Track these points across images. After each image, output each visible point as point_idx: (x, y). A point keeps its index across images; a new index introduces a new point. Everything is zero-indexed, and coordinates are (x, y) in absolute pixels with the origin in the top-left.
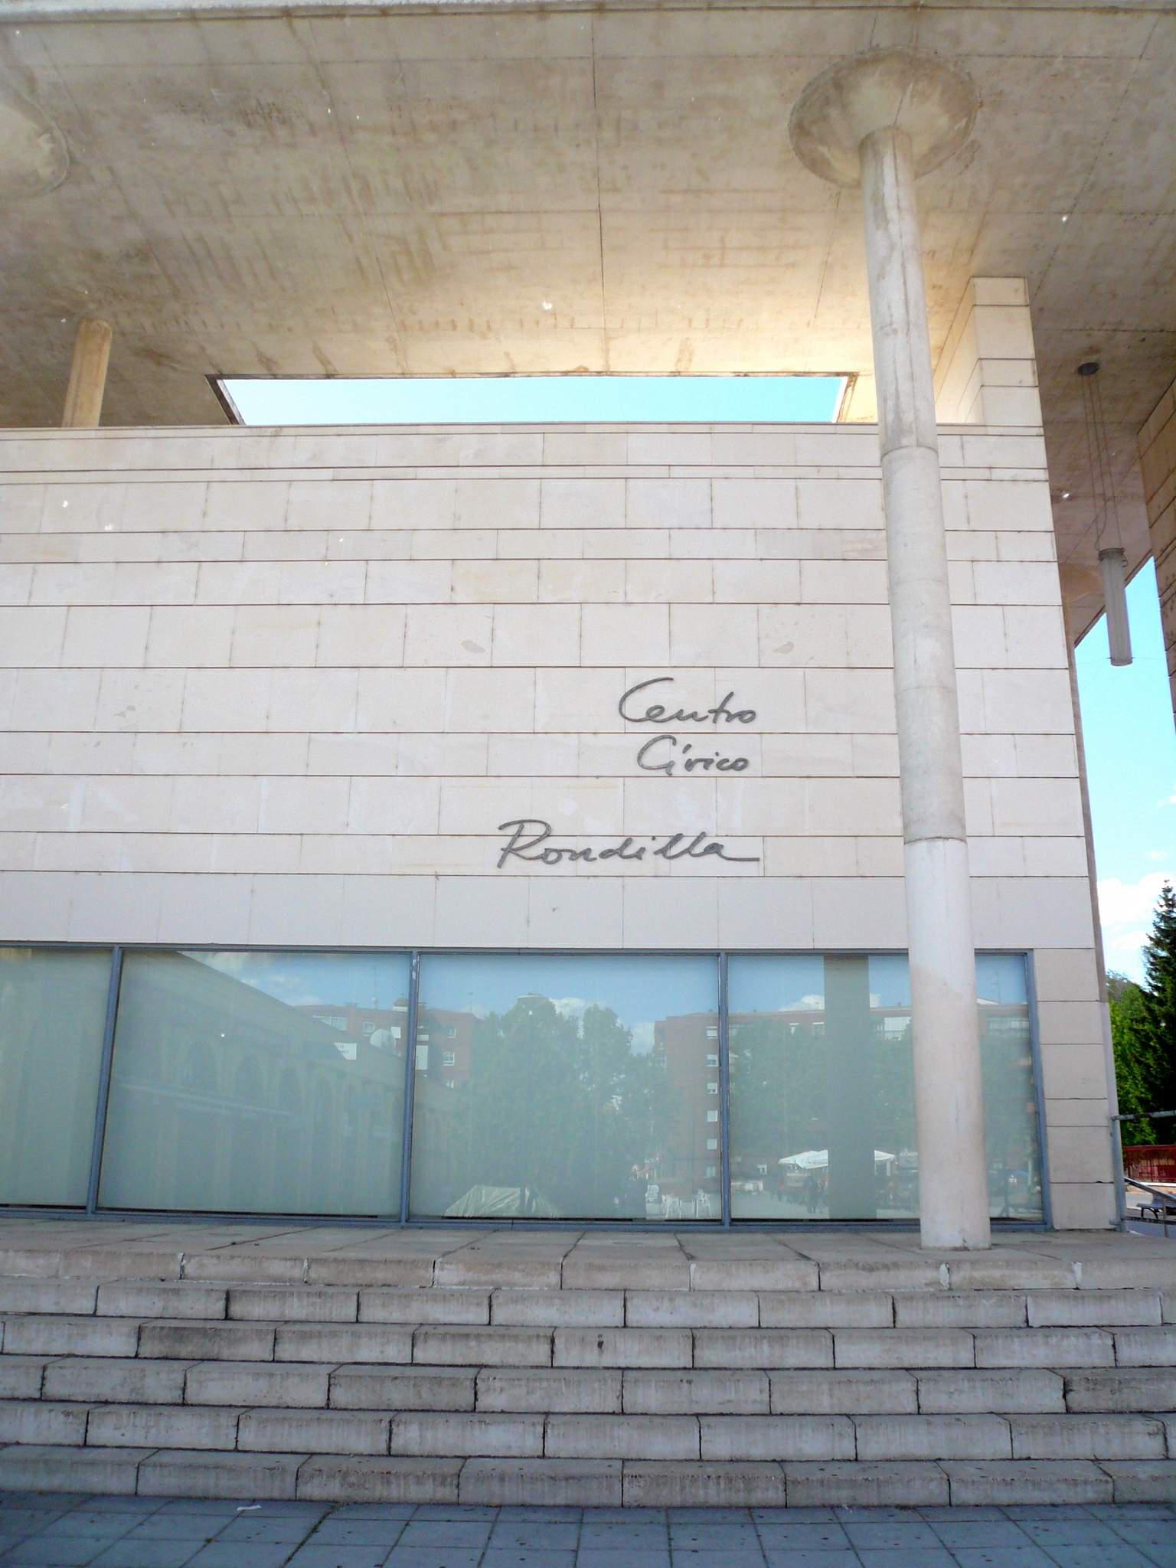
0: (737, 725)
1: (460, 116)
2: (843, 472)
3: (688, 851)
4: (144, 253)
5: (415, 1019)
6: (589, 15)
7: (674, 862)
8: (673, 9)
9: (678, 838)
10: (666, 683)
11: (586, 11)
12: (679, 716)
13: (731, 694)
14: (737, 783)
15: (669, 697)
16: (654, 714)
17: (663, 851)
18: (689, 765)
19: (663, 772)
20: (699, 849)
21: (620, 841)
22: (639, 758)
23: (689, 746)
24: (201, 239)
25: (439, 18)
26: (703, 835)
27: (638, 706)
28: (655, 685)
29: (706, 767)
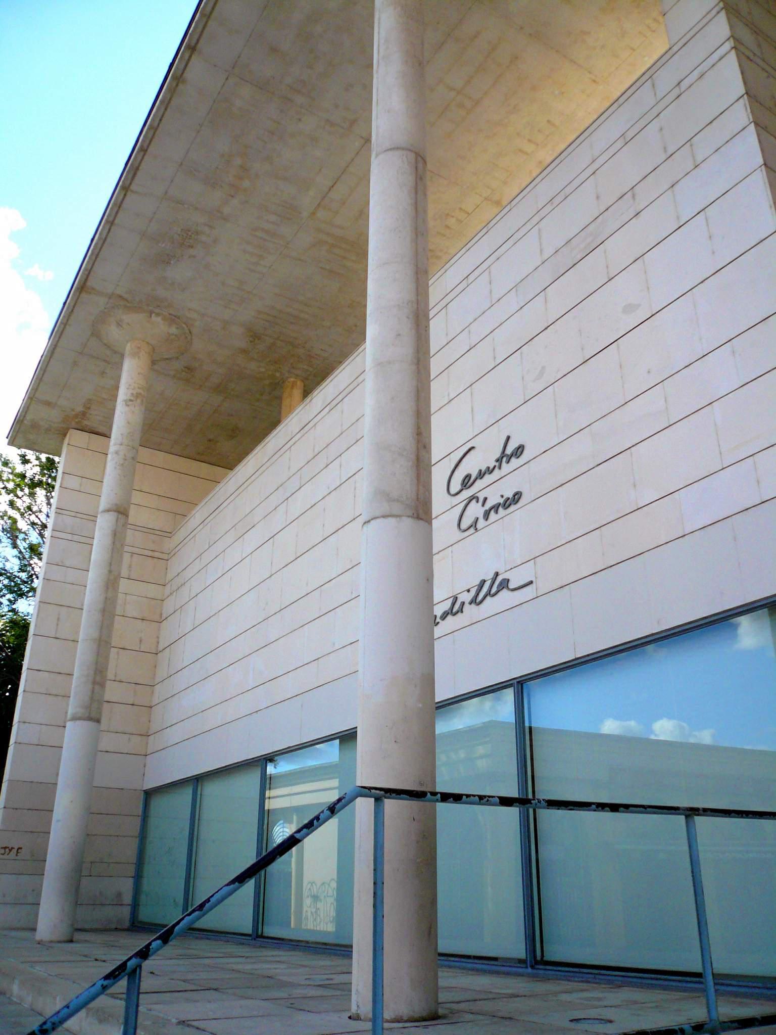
0: (515, 462)
1: (238, 161)
2: (568, 190)
3: (488, 594)
4: (255, 336)
5: (525, 736)
6: (193, 56)
7: (482, 605)
8: (213, 8)
9: (484, 582)
10: (472, 452)
11: (190, 56)
12: (481, 475)
13: (508, 438)
14: (516, 513)
15: (471, 466)
16: (467, 482)
17: (474, 601)
18: (487, 515)
19: (472, 530)
20: (494, 590)
21: (450, 602)
22: (459, 525)
23: (485, 499)
24: (259, 312)
25: (160, 129)
26: (497, 574)
27: (456, 486)
28: (464, 460)
29: (497, 512)
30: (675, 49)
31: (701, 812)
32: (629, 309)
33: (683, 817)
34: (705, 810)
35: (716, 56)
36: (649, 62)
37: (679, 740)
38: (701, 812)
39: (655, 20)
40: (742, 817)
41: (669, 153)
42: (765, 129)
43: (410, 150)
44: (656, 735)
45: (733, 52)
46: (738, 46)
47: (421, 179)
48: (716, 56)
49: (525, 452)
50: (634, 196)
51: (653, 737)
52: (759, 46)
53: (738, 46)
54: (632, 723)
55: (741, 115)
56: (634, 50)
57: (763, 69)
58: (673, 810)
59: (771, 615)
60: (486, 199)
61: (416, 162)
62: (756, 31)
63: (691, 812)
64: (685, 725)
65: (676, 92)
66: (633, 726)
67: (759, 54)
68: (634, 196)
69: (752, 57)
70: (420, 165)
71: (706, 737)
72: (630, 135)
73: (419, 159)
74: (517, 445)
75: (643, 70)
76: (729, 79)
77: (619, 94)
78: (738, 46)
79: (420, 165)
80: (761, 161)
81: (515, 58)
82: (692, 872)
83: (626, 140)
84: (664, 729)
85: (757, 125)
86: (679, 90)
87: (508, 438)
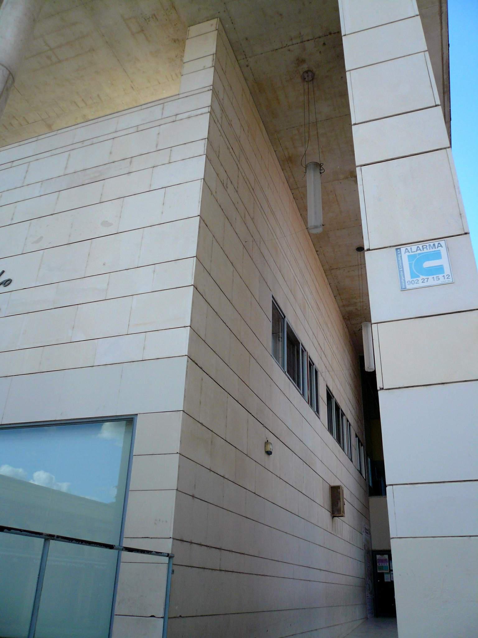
2: (95, 140)
30: (181, 96)
31: (55, 538)
32: (106, 224)
33: (43, 540)
34: (58, 537)
35: (199, 112)
36: (165, 96)
37: (44, 486)
38: (55, 538)
39: (176, 75)
40: (79, 544)
41: (158, 149)
42: (210, 160)
43: (7, 69)
44: (34, 481)
45: (209, 114)
46: (212, 113)
47: (7, 90)
48: (199, 112)
49: (12, 283)
50: (131, 162)
51: (31, 482)
52: (222, 118)
53: (212, 113)
54: (20, 470)
55: (201, 148)
56: (159, 83)
57: (230, 152)
58: (38, 534)
59: (127, 425)
60: (43, 120)
61: (8, 78)
62: (223, 110)
63: (50, 537)
64: (54, 477)
65: (173, 118)
66: (20, 472)
67: (220, 121)
68: (131, 162)
69: (216, 121)
70: (10, 82)
71: (64, 487)
72: (141, 128)
73: (11, 77)
74: (7, 279)
75: (160, 98)
76: (201, 127)
77: (144, 103)
78: (212, 113)
79: (10, 82)
80: (202, 177)
81: (92, 50)
82: (39, 575)
83: (138, 130)
84: (40, 478)
85: (207, 156)
86: (175, 119)
87: (3, 272)
